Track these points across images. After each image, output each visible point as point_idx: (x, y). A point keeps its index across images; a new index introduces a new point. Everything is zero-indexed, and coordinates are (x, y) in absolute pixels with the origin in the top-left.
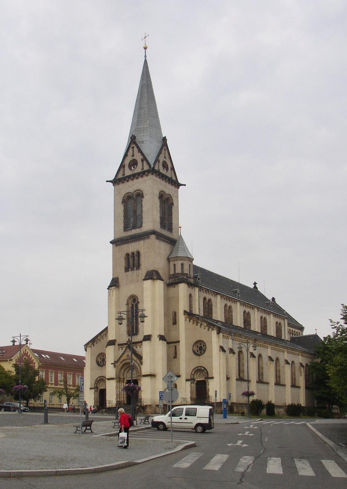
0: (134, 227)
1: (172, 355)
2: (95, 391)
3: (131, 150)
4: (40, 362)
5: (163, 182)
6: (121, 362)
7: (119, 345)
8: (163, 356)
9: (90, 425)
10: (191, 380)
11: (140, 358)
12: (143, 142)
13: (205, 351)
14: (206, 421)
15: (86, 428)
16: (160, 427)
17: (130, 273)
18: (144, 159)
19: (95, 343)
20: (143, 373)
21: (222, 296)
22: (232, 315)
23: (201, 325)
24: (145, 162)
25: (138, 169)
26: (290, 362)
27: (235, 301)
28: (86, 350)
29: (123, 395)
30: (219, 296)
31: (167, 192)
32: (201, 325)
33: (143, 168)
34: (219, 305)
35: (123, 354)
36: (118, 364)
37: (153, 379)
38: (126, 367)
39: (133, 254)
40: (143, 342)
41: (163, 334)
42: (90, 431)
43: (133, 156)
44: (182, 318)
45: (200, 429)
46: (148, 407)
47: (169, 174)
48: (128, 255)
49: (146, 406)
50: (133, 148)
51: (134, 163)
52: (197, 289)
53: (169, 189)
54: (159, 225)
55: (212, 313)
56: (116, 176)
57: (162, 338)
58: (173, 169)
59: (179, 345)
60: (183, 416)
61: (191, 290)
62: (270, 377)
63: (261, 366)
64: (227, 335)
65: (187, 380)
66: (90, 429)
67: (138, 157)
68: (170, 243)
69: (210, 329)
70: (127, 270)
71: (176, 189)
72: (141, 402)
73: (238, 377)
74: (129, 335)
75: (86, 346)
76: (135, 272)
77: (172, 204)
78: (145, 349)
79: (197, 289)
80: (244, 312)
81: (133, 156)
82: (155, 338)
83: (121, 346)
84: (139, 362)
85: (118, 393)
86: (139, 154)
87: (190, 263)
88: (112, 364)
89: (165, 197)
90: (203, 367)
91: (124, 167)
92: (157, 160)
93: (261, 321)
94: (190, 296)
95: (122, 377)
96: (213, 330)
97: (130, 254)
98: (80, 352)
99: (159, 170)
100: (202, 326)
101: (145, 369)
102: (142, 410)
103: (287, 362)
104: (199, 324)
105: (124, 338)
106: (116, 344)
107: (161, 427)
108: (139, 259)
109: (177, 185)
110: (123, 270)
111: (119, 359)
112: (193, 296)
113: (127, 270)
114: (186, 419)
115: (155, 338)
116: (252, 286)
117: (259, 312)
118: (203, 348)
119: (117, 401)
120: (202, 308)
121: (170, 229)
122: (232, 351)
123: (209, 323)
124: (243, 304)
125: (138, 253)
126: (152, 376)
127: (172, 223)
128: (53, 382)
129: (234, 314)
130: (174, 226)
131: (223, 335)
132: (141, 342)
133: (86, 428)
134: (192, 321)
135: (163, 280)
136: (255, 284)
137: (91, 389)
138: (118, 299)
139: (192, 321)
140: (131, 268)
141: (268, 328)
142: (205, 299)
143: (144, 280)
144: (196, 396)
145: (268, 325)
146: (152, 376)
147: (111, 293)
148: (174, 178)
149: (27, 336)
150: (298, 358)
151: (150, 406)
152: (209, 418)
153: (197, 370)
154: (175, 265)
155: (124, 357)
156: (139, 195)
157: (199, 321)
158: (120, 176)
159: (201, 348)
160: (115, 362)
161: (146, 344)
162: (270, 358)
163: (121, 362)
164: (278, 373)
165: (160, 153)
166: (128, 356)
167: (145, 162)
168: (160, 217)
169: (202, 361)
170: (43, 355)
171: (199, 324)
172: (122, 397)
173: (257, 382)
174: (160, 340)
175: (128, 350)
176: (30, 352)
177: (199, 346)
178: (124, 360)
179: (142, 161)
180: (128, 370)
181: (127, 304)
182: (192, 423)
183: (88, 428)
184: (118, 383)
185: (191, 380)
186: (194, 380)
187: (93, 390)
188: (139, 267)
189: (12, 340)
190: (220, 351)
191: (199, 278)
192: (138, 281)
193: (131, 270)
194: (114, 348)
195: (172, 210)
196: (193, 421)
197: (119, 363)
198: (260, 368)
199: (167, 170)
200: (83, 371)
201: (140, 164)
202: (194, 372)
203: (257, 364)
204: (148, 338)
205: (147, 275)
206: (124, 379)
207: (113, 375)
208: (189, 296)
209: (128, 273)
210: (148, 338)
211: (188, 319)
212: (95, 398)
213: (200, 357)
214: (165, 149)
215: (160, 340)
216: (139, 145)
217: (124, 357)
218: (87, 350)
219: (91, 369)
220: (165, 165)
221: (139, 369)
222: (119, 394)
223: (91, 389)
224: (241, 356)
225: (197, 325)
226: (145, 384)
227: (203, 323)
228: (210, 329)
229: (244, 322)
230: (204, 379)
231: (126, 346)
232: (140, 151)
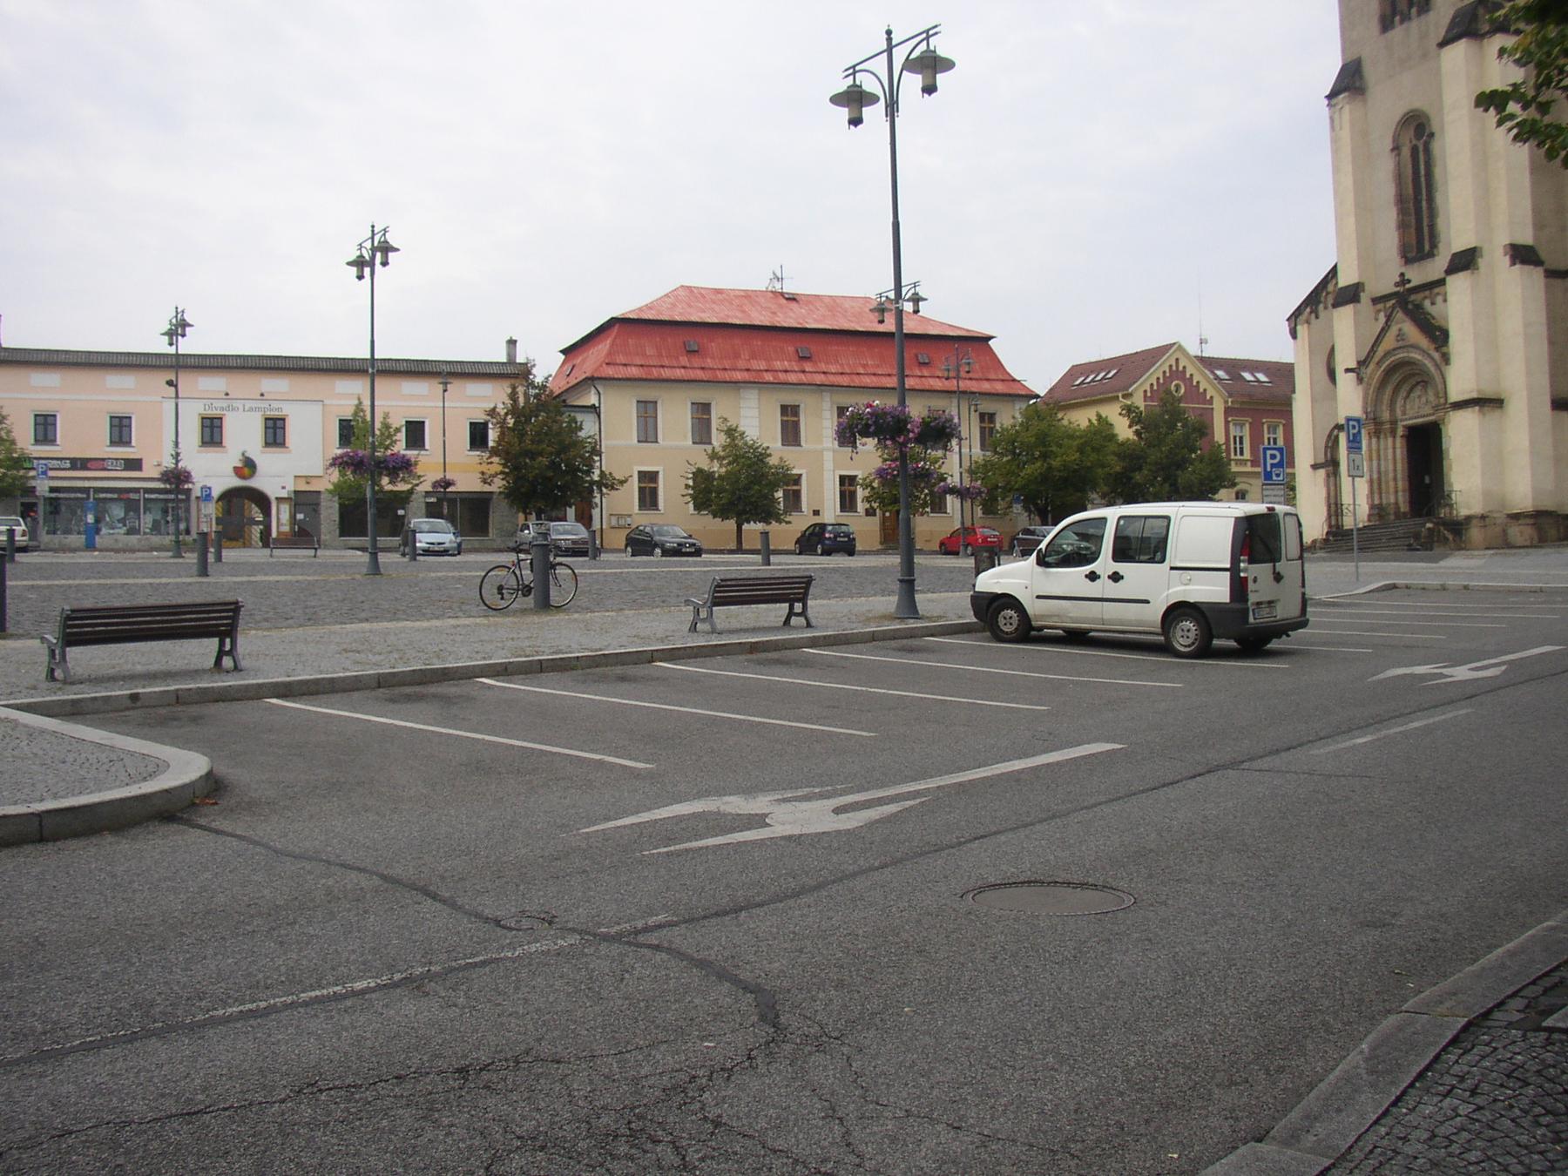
2: (1328, 476)
4: (1230, 395)
6: (1379, 364)
7: (1375, 301)
8: (1527, 325)
9: (803, 599)
11: (1439, 336)
14: (1215, 590)
15: (791, 607)
16: (1001, 621)
17: (1397, 33)
20: (1454, 397)
28: (1294, 334)
29: (1392, 484)
35: (1384, 331)
36: (1369, 370)
37: (1493, 415)
38: (1396, 378)
40: (1449, 279)
41: (1526, 237)
42: (802, 620)
45: (1186, 634)
46: (1475, 522)
49: (1469, 518)
57: (1522, 255)
60: (1105, 563)
66: (803, 613)
70: (1386, 24)
72: (1451, 506)
75: (1295, 318)
76: (1415, 25)
78: (1458, 305)
82: (1496, 261)
83: (1380, 306)
84: (1436, 355)
85: (1375, 476)
95: (1386, 416)
98: (1277, 347)
101: (1461, 380)
102: (1450, 537)
105: (1386, 274)
106: (1365, 297)
107: (1008, 620)
111: (1373, 350)
113: (1386, 24)
114: (1116, 577)
115: (1496, 261)
119: (1372, 507)
126: (1488, 403)
128: (1247, 455)
133: (791, 607)
138: (1362, 135)
140: (1402, 14)
146: (1488, 403)
147: (1336, 116)
151: (1483, 517)
152: (1234, 570)
155: (1389, 342)
161: (1458, 286)
163: (1379, 364)
166: (1400, 336)
170: (1247, 376)
172: (1392, 490)
174: (1513, 263)
175: (1400, 315)
176: (1193, 363)
178: (1387, 354)
180: (1406, 387)
181: (1396, 148)
182: (1147, 602)
183: (798, 607)
184: (1374, 440)
187: (1322, 472)
189: (352, 258)
192: (1425, 56)
193: (1402, 22)
194: (1356, 313)
196: (1151, 589)
197: (1372, 366)
200: (1291, 412)
204: (1465, 261)
205: (1453, 23)
206: (1394, 422)
209: (1390, 34)
210: (1465, 261)
215: (1513, 263)
217: (1389, 342)
218: (1299, 335)
219: (1314, 400)
222: (1379, 479)
223: (1315, 467)
226: (1463, 438)
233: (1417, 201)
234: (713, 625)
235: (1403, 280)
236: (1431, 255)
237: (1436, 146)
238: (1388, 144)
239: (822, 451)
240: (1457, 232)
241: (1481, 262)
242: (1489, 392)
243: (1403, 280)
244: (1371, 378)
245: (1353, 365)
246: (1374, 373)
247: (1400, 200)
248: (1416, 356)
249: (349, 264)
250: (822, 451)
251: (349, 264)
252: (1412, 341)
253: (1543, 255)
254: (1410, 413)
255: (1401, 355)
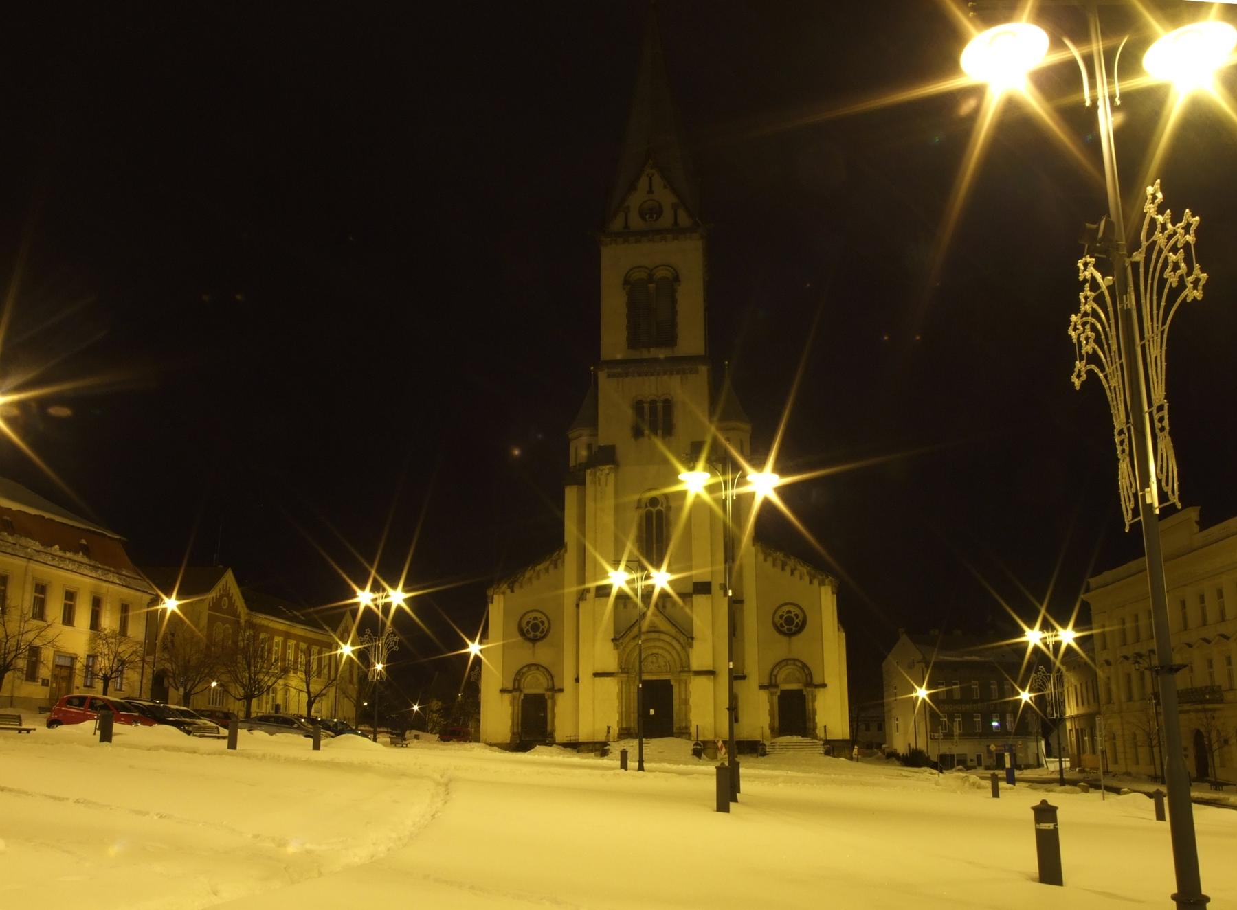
10: (769, 685)
19: (517, 585)
43: (651, 191)
59: (742, 610)
69: (816, 582)
96: (822, 583)
100: (797, 573)
104: (788, 569)
137: (503, 691)
139: (770, 560)
146: (711, 673)
169: (799, 646)
171: (788, 569)
185: (769, 686)
186: (776, 686)
187: (507, 696)
191: (1153, 202)
211: (761, 557)
212: (513, 714)
223: (503, 691)
225: (783, 569)
228: (816, 582)
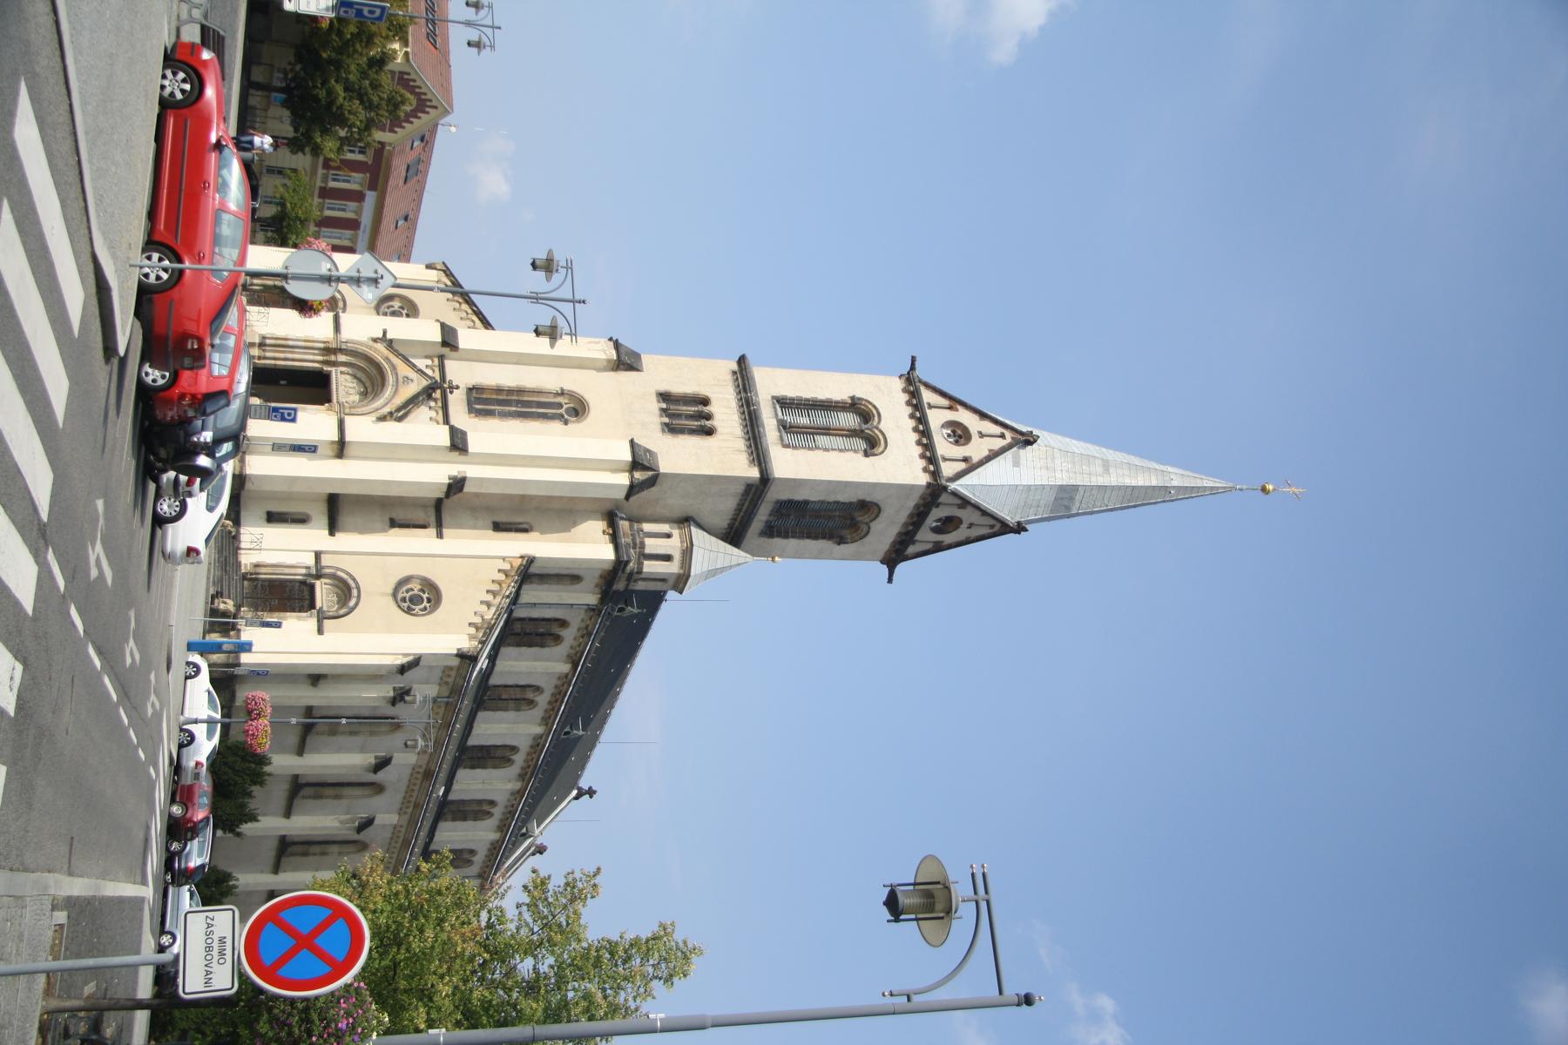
0: (784, 427)
1: (400, 515)
3: (998, 430)
5: (903, 516)
6: (387, 359)
12: (1016, 463)
13: (409, 611)
17: (655, 406)
18: (971, 466)
19: (450, 296)
20: (348, 420)
21: (565, 679)
22: (506, 709)
23: (494, 594)
24: (963, 466)
25: (943, 447)
26: (381, 776)
27: (546, 720)
30: (565, 668)
31: (876, 526)
32: (488, 605)
33: (945, 459)
34: (540, 666)
38: (373, 371)
39: (709, 417)
43: (982, 435)
44: (516, 547)
47: (925, 535)
48: (705, 401)
50: (1002, 436)
51: (960, 435)
52: (592, 599)
53: (884, 532)
54: (785, 496)
55: (518, 645)
56: (927, 386)
58: (938, 548)
61: (591, 581)
62: (310, 821)
63: (347, 791)
64: (450, 680)
65: (318, 555)
67: (977, 449)
68: (731, 526)
69: (472, 631)
70: (664, 397)
71: (881, 555)
73: (301, 781)
74: (470, 390)
77: (841, 541)
78: (425, 428)
79: (592, 599)
80: (514, 749)
81: (982, 435)
84: (387, 410)
86: (986, 453)
87: (671, 582)
88: (385, 333)
89: (861, 518)
90: (357, 604)
91: (950, 408)
92: (964, 502)
93: (480, 802)
94: (575, 579)
96: (472, 637)
97: (706, 409)
99: (938, 506)
100: (484, 608)
101: (361, 429)
103: (382, 764)
104: (489, 598)
105: (461, 373)
108: (693, 432)
109: (893, 559)
110: (663, 388)
112: (577, 587)
116: (584, 783)
117: (507, 796)
118: (417, 608)
120: (536, 614)
121: (770, 531)
122: (401, 696)
123: (491, 628)
124: (537, 743)
125: (709, 432)
127: (786, 537)
128: (332, 184)
129: (511, 715)
130: (778, 542)
131: (451, 668)
132: (446, 421)
134: (502, 577)
135: (627, 497)
136: (591, 792)
141: (459, 824)
142: (563, 623)
143: (632, 442)
144: (264, 580)
145: (470, 823)
148: (911, 550)
149: (492, 47)
150: (389, 812)
153: (349, 589)
154: (669, 536)
156: (872, 444)
157: (498, 599)
158: (927, 396)
159: (415, 600)
160: (391, 341)
162: (368, 823)
164: (316, 849)
165: (985, 513)
166: (407, 379)
167: (963, 466)
168: (806, 502)
171: (495, 587)
173: (296, 777)
175: (425, 383)
177: (425, 596)
178: (394, 368)
179: (965, 460)
180: (364, 378)
188: (671, 429)
189: (556, 257)
190: (406, 655)
195: (824, 538)
197: (386, 352)
198: (337, 790)
199: (936, 530)
201: (960, 451)
202: (344, 576)
203: (353, 779)
206: (334, 364)
207: (346, 334)
208: (576, 572)
209: (654, 398)
213: (391, 599)
214: (992, 527)
216: (1009, 454)
220: (949, 524)
221: (365, 409)
224: (366, 791)
227: (493, 609)
229: (481, 748)
230: (318, 604)
231: (437, 376)
232: (993, 455)
233: (518, 402)
234: (187, 22)
235: (452, 388)
236: (471, 410)
237: (556, 426)
238: (567, 387)
239: (135, 967)
240: (486, 435)
241: (455, 454)
242: (349, 450)
243: (452, 388)
244: (376, 350)
245: (389, 336)
246: (380, 352)
247: (520, 391)
248: (388, 392)
249: (550, 252)
250: (135, 967)
251: (550, 252)
252: (401, 390)
253: (455, 498)
254: (342, 378)
255: (391, 379)
